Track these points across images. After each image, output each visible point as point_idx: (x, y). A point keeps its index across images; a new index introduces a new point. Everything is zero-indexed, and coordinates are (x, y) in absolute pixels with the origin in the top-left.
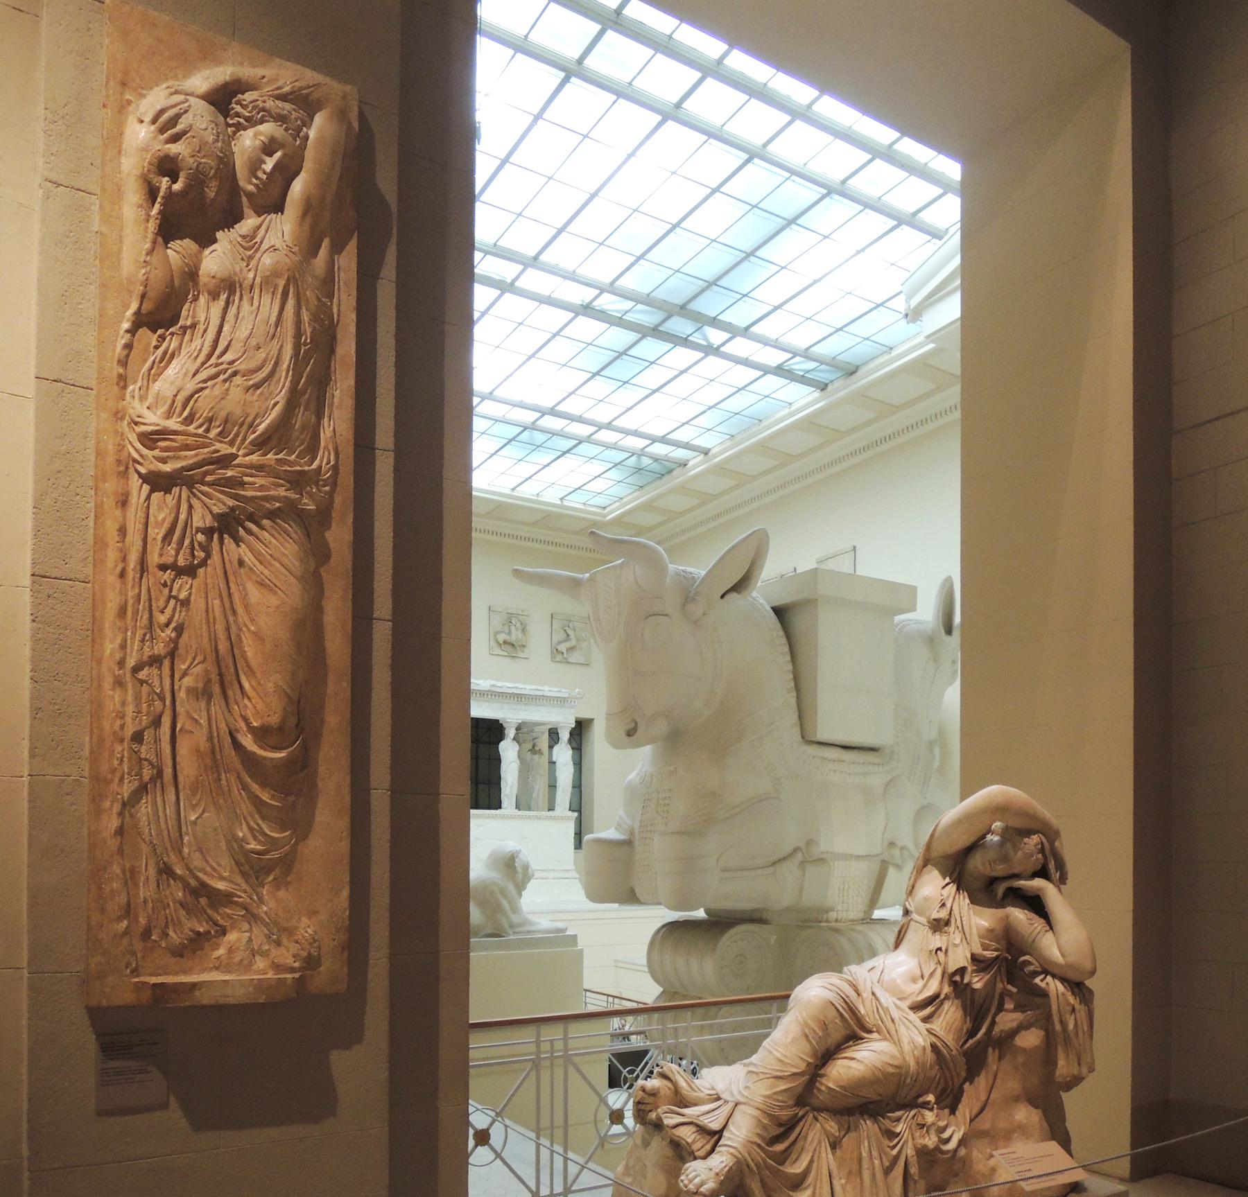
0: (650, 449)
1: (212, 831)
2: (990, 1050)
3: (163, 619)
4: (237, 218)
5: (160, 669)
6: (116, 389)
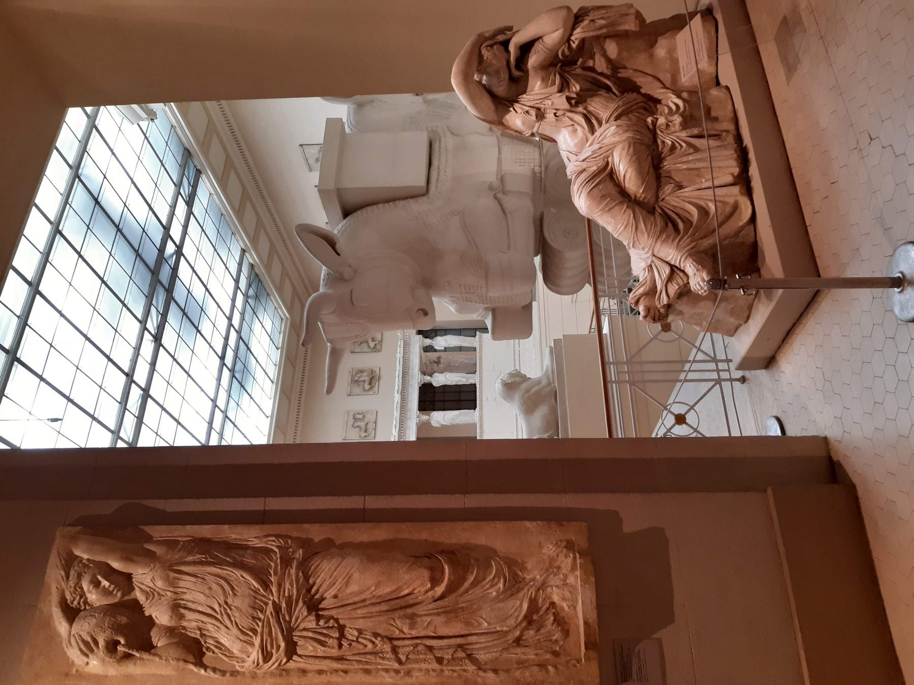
1: (495, 611)
2: (619, 75)
3: (370, 646)
4: (136, 601)
5: (399, 647)
6: (239, 677)
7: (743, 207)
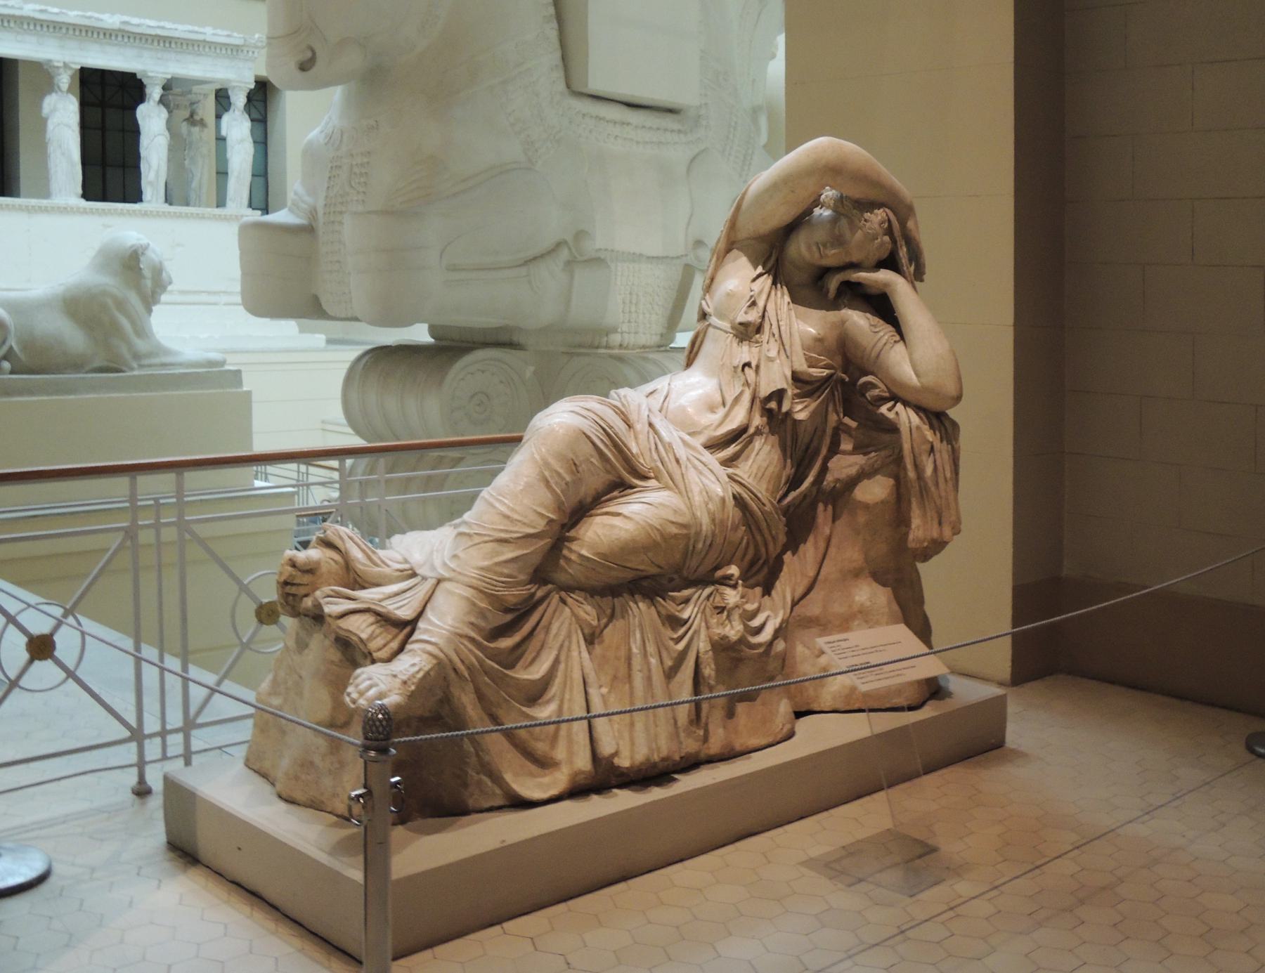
2: (821, 506)
7: (546, 780)
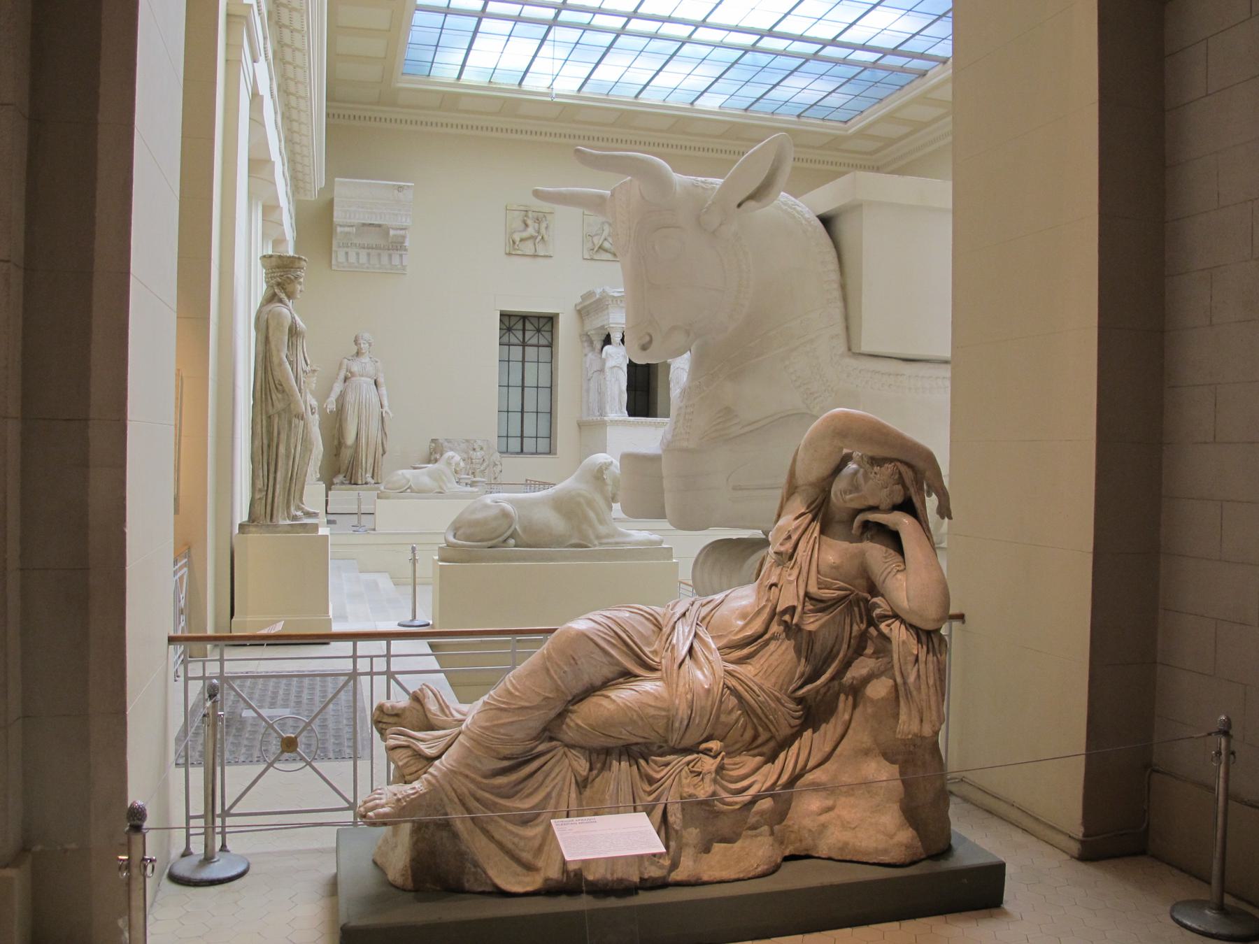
0: (884, 62)
2: (842, 697)
7: (527, 879)
